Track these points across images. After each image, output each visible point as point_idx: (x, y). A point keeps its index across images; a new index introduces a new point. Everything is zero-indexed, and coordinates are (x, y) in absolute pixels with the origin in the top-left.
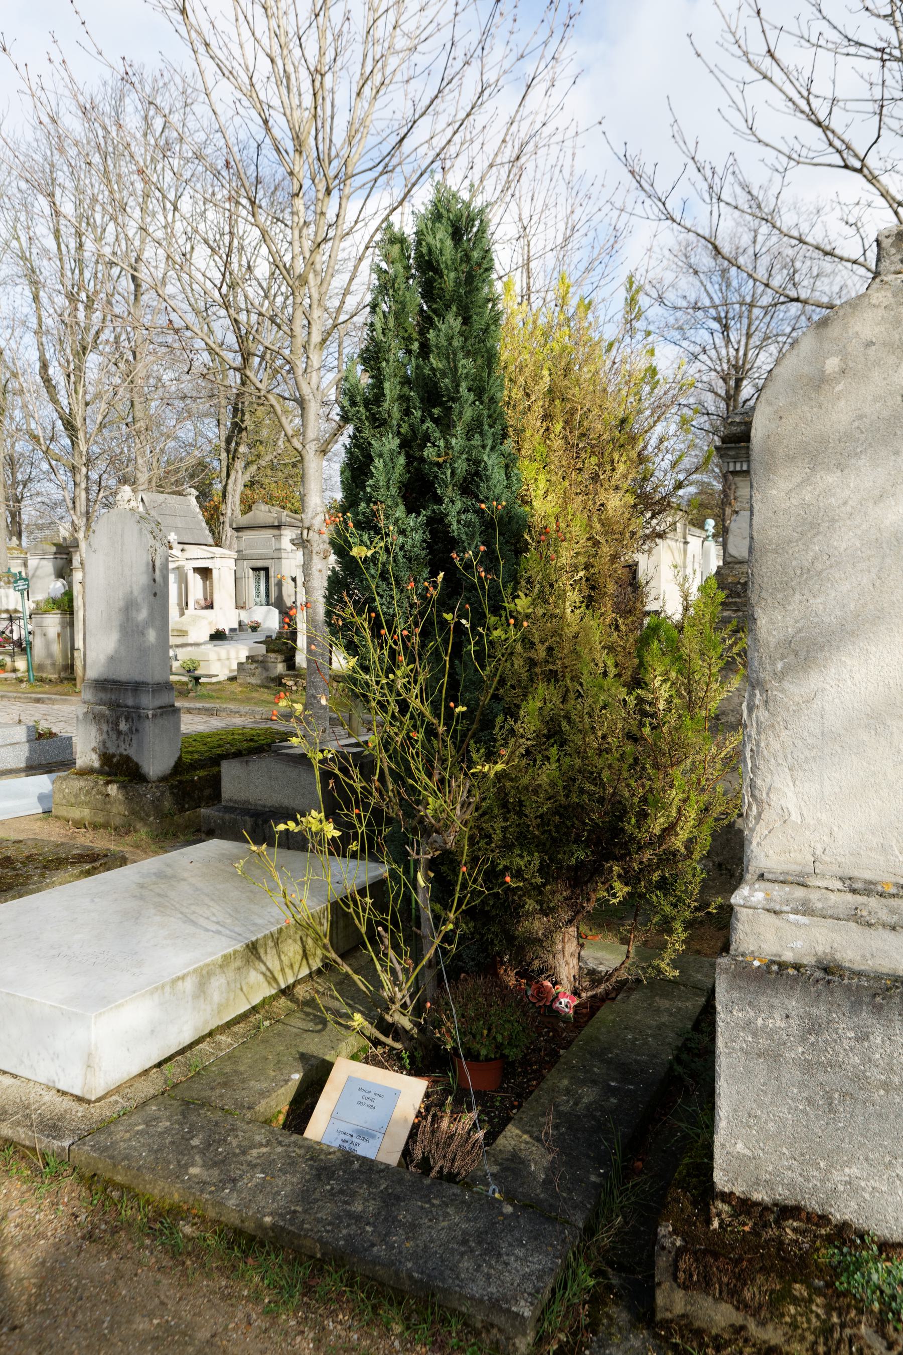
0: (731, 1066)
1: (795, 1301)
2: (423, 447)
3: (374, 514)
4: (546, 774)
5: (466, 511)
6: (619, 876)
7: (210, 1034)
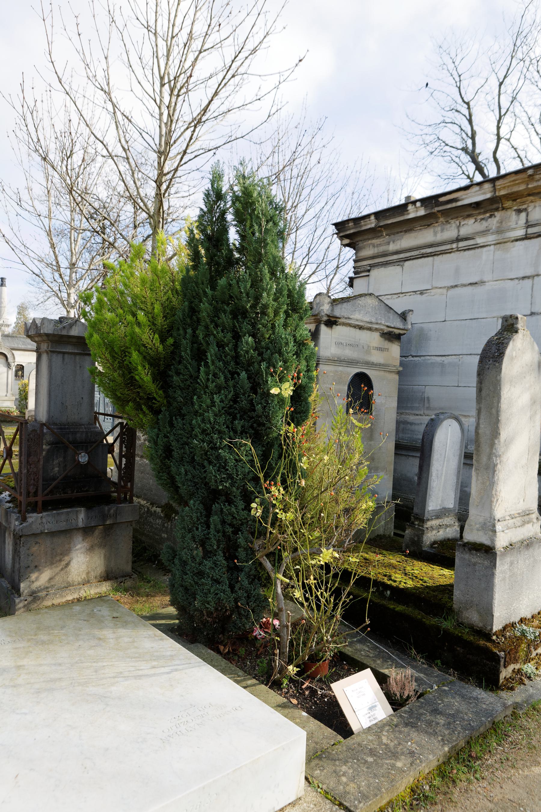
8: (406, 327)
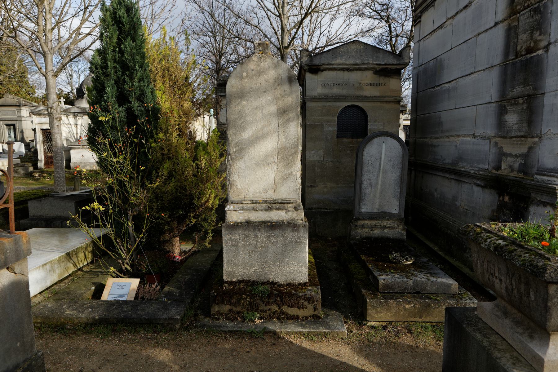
0: (227, 250)
1: (243, 299)
2: (124, 85)
3: (108, 106)
4: (171, 186)
5: (140, 106)
6: (193, 217)
7: (56, 283)
8: (401, 62)
